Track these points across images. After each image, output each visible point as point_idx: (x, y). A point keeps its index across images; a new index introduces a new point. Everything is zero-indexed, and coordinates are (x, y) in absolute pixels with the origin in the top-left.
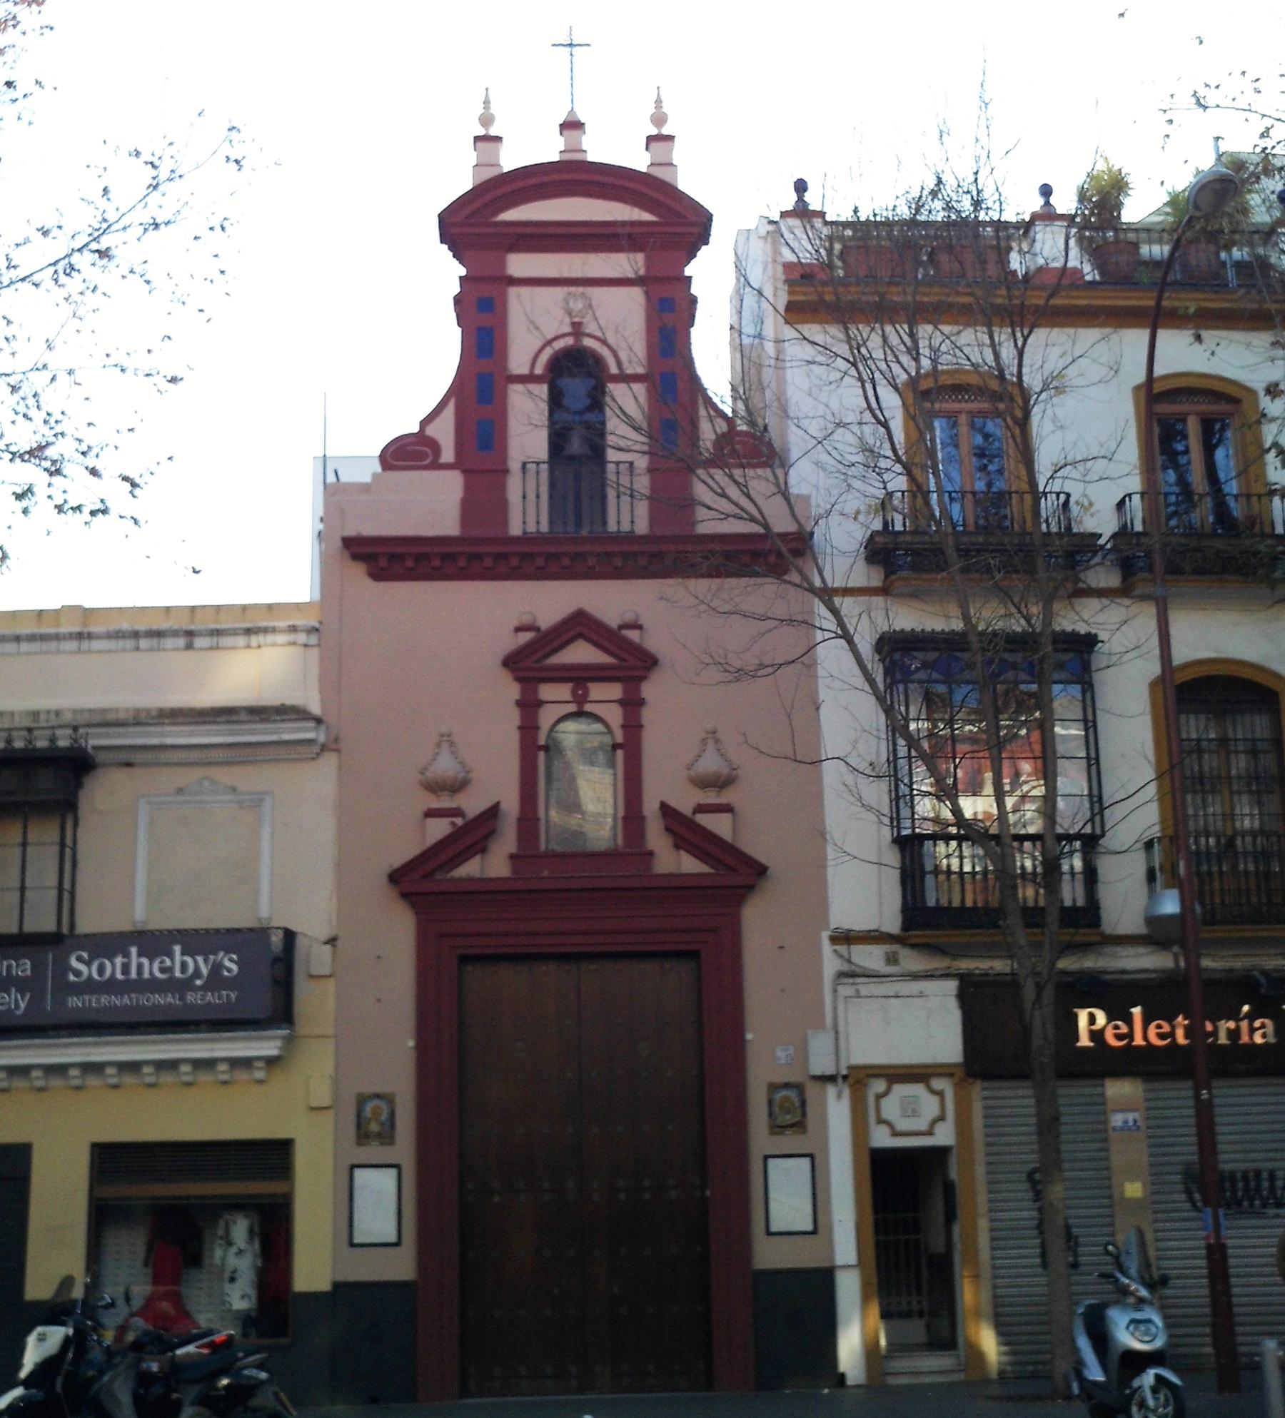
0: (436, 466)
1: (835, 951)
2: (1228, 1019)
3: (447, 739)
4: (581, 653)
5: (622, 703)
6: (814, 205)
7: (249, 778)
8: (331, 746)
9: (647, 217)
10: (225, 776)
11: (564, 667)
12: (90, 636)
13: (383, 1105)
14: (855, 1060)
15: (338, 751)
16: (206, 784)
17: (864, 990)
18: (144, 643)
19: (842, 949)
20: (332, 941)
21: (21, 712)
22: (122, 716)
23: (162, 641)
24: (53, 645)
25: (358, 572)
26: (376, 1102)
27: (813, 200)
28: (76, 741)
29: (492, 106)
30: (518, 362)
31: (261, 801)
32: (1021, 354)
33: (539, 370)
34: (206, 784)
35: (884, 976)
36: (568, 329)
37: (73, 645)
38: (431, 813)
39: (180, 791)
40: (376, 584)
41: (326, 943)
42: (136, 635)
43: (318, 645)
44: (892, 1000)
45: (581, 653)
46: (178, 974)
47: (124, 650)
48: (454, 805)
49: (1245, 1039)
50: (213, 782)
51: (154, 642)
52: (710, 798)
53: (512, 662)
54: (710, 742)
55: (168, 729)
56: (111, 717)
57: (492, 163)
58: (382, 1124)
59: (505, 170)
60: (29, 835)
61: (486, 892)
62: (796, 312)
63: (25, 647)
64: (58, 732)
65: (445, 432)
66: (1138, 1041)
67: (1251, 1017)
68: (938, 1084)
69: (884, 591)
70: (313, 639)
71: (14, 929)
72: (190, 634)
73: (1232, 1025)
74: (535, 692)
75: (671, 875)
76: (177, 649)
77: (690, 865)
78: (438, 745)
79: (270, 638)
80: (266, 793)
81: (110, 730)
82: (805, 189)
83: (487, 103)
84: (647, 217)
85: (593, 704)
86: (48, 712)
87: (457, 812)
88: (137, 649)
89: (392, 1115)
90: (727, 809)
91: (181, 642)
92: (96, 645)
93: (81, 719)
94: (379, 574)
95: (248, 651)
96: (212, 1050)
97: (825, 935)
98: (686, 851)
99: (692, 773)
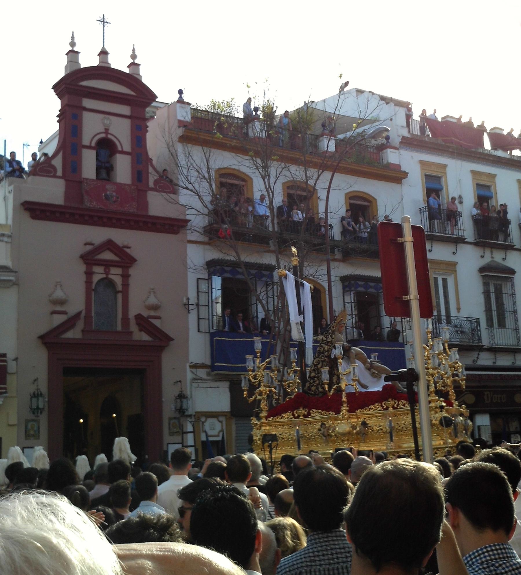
0: (55, 176)
1: (191, 371)
4: (107, 256)
5: (122, 276)
8: (15, 284)
9: (132, 93)
13: (35, 423)
14: (199, 409)
15: (18, 285)
17: (201, 385)
19: (194, 370)
20: (16, 359)
25: (27, 214)
26: (32, 423)
29: (75, 39)
30: (86, 141)
32: (319, 176)
33: (93, 144)
35: (207, 380)
38: (54, 312)
41: (13, 360)
43: (11, 242)
44: (209, 389)
45: (107, 256)
52: (152, 313)
57: (137, 73)
61: (73, 344)
62: (184, 139)
65: (58, 163)
68: (221, 419)
70: (9, 240)
77: (145, 337)
78: (150, 292)
84: (132, 93)
87: (65, 313)
89: (39, 427)
97: (188, 365)
99: (51, 298)
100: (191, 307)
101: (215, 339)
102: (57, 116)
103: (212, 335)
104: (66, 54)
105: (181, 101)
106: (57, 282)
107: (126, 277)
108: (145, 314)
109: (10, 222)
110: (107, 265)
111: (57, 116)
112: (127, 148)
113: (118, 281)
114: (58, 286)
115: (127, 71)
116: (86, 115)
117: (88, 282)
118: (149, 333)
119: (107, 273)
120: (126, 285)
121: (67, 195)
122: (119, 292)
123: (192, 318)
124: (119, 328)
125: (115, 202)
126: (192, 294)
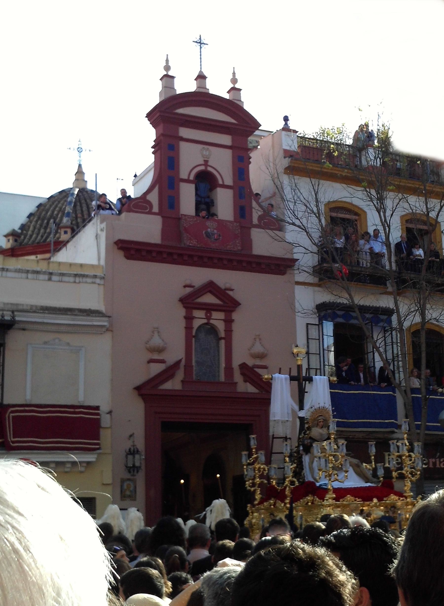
0: (150, 213)
2: (433, 458)
3: (156, 330)
4: (209, 299)
5: (225, 321)
6: (292, 127)
9: (233, 121)
10: (66, 338)
11: (205, 304)
12: (7, 270)
16: (57, 341)
18: (30, 276)
20: (110, 412)
22: (25, 307)
25: (121, 254)
27: (292, 125)
33: (192, 178)
34: (57, 341)
36: (203, 163)
39: (45, 343)
40: (126, 260)
41: (108, 413)
42: (27, 272)
43: (104, 285)
45: (209, 299)
47: (21, 278)
48: (161, 358)
49: (438, 466)
50: (60, 340)
51: (35, 276)
53: (182, 300)
54: (258, 340)
55: (46, 315)
56: (20, 307)
58: (131, 491)
59: (178, 92)
64: (5, 313)
65: (154, 198)
66: (438, 466)
67: (440, 458)
69: (319, 286)
70: (102, 282)
72: (51, 274)
73: (434, 460)
74: (191, 313)
75: (244, 393)
76: (45, 280)
77: (251, 389)
78: (153, 332)
79: (85, 279)
80: (82, 347)
81: (25, 314)
82: (288, 120)
83: (167, 61)
85: (214, 320)
87: (162, 361)
88: (27, 278)
89: (135, 487)
90: (265, 367)
91: (46, 277)
92: (9, 274)
93: (15, 308)
94: (129, 257)
95: (74, 284)
98: (250, 383)
99: (148, 346)
102: (152, 147)
105: (286, 128)
107: (229, 322)
108: (250, 362)
111: (152, 147)
112: (229, 181)
113: (221, 326)
116: (183, 146)
117: (188, 328)
119: (208, 318)
120: (229, 331)
122: (221, 338)
125: (216, 240)
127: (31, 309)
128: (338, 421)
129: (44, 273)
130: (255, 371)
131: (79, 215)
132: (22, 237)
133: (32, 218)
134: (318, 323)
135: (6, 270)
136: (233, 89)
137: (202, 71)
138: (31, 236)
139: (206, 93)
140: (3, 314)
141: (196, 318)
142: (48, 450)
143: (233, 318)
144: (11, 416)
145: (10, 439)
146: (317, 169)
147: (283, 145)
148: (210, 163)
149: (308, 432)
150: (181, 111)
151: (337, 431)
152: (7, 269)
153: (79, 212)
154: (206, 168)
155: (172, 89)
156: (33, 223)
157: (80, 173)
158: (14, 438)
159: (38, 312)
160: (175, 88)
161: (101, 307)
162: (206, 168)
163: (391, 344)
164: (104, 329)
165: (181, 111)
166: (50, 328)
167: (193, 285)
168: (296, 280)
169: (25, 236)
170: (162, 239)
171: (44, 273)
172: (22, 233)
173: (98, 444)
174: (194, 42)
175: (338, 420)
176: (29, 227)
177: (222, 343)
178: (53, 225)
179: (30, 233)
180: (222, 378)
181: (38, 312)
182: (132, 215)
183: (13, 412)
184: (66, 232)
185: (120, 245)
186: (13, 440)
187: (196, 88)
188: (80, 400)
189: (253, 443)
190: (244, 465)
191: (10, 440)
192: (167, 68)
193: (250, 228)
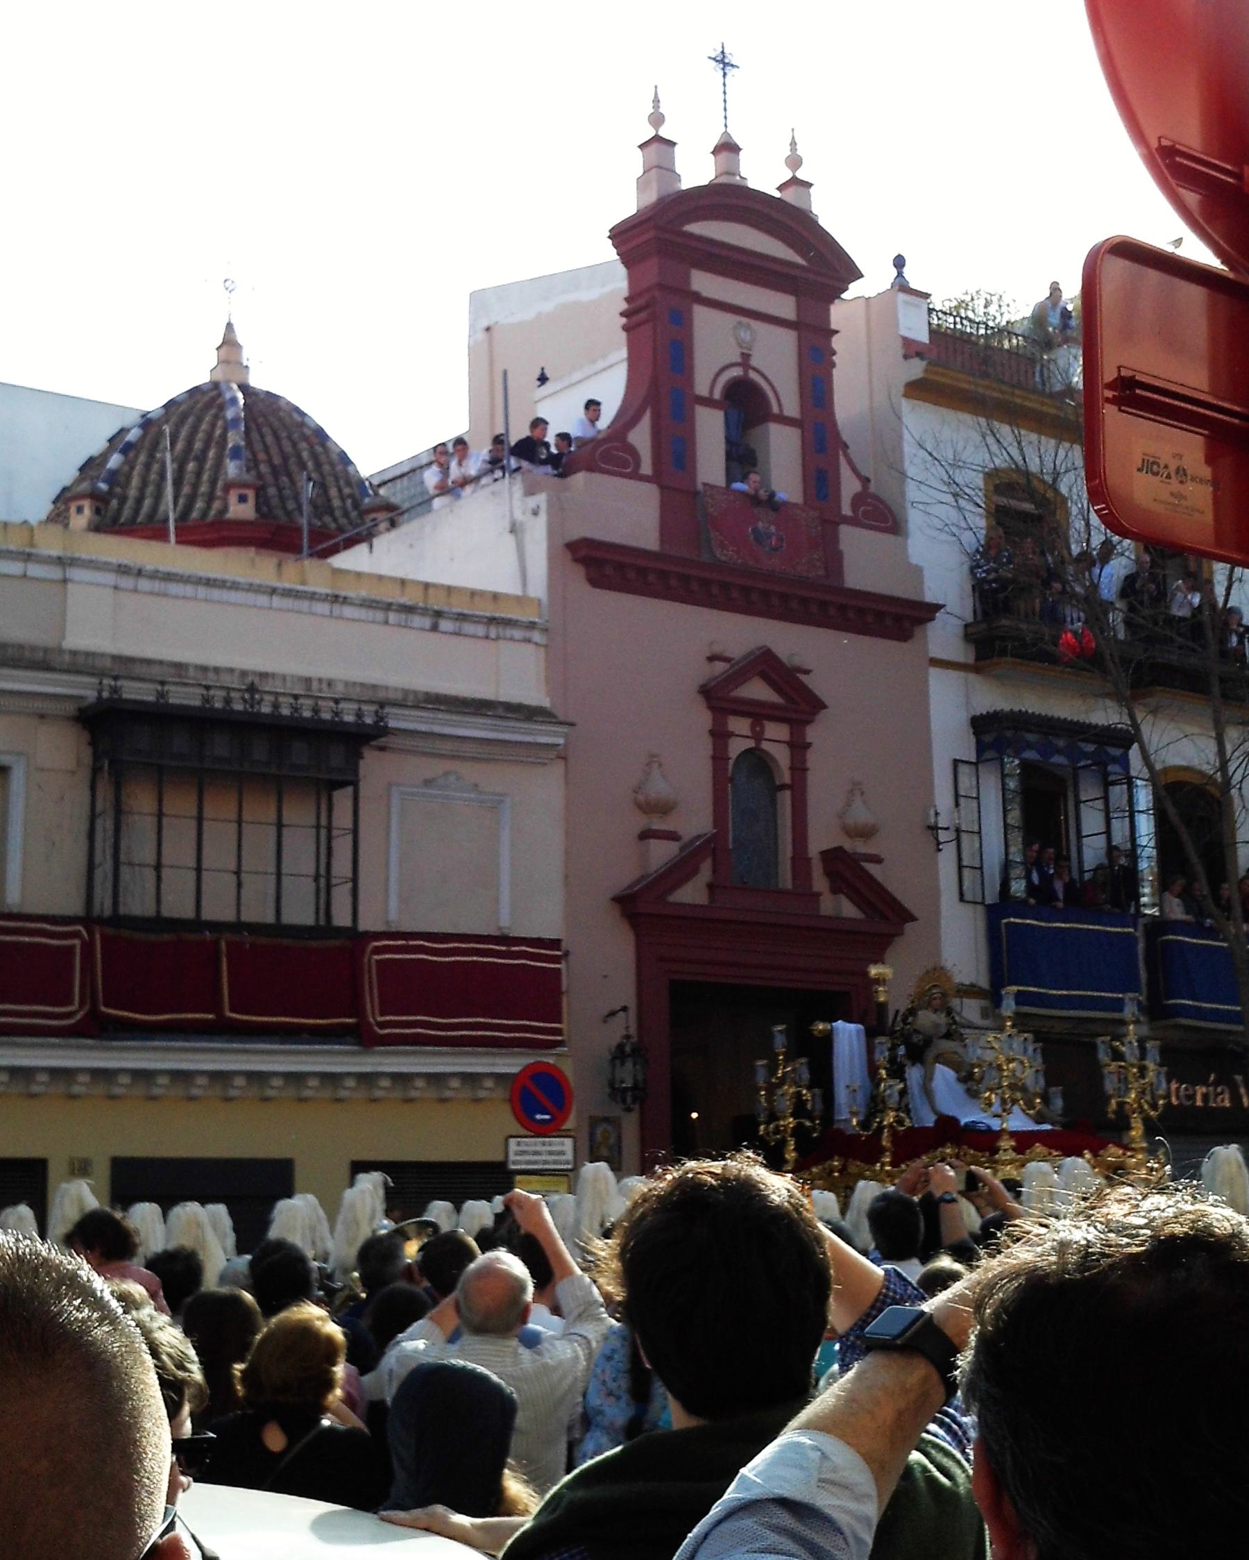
0: (636, 476)
4: (757, 690)
7: (494, 778)
9: (799, 260)
10: (469, 771)
12: (345, 601)
16: (452, 778)
18: (392, 617)
21: (292, 676)
23: (410, 616)
24: (304, 605)
25: (578, 574)
28: (296, 710)
30: (702, 389)
31: (501, 802)
33: (717, 395)
36: (739, 360)
37: (322, 608)
38: (646, 835)
39: (428, 783)
42: (388, 607)
43: (546, 646)
45: (757, 690)
46: (1199, 1103)
47: (373, 622)
57: (667, 166)
60: (285, 813)
61: (688, 919)
63: (277, 601)
64: (320, 703)
65: (640, 438)
71: (270, 918)
72: (438, 614)
73: (1204, 1090)
76: (423, 629)
77: (849, 910)
79: (509, 632)
83: (656, 101)
86: (320, 680)
87: (672, 836)
88: (386, 622)
89: (619, 1139)
91: (427, 622)
92: (348, 611)
96: (493, 1065)
98: (848, 896)
99: (641, 798)
100: (943, 836)
101: (1005, 921)
102: (622, 314)
103: (994, 914)
104: (640, 147)
105: (901, 285)
106: (653, 756)
107: (799, 747)
109: (538, 588)
110: (758, 713)
111: (622, 314)
112: (791, 407)
113: (781, 755)
114: (655, 765)
115: (777, 194)
116: (701, 314)
117: (719, 758)
118: (858, 899)
119: (758, 736)
120: (799, 769)
121: (666, 529)
122: (783, 787)
123: (946, 862)
124: (788, 885)
125: (775, 549)
126: (943, 799)
127: (404, 700)
128: (1019, 991)
129: (424, 611)
130: (863, 870)
131: (262, 456)
132: (114, 503)
133: (131, 455)
134: (974, 761)
135: (341, 600)
136: (794, 181)
137: (728, 131)
138: (139, 501)
139: (738, 186)
140: (360, 709)
141: (737, 736)
142: (453, 1045)
143: (808, 740)
144: (373, 962)
145: (374, 1018)
146: (965, 386)
147: (901, 326)
148: (754, 362)
149: (910, 1019)
150: (696, 228)
151: (1017, 1014)
152: (345, 598)
153: (258, 447)
154: (746, 372)
155: (669, 173)
156: (138, 468)
157: (229, 344)
158: (382, 1015)
159: (424, 708)
160: (678, 171)
161: (535, 696)
162: (746, 372)
163: (1127, 814)
164: (553, 754)
165: (696, 228)
166: (447, 747)
167: (728, 654)
168: (932, 655)
169: (123, 500)
170: (663, 541)
171: (424, 611)
172: (110, 493)
173: (558, 1032)
174: (710, 58)
175: (1021, 988)
176: (129, 478)
177: (785, 798)
178: (307, 485)
179: (132, 493)
180: (786, 879)
181: (424, 708)
182: (597, 477)
183: (378, 951)
184: (243, 499)
185: (583, 552)
186: (380, 1019)
187: (713, 177)
188: (502, 924)
189: (780, 1043)
190: (760, 1089)
191: (371, 1020)
192: (657, 119)
193: (838, 524)
